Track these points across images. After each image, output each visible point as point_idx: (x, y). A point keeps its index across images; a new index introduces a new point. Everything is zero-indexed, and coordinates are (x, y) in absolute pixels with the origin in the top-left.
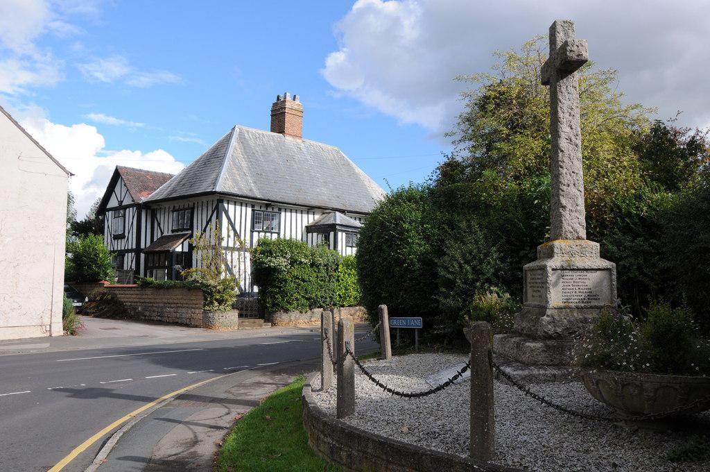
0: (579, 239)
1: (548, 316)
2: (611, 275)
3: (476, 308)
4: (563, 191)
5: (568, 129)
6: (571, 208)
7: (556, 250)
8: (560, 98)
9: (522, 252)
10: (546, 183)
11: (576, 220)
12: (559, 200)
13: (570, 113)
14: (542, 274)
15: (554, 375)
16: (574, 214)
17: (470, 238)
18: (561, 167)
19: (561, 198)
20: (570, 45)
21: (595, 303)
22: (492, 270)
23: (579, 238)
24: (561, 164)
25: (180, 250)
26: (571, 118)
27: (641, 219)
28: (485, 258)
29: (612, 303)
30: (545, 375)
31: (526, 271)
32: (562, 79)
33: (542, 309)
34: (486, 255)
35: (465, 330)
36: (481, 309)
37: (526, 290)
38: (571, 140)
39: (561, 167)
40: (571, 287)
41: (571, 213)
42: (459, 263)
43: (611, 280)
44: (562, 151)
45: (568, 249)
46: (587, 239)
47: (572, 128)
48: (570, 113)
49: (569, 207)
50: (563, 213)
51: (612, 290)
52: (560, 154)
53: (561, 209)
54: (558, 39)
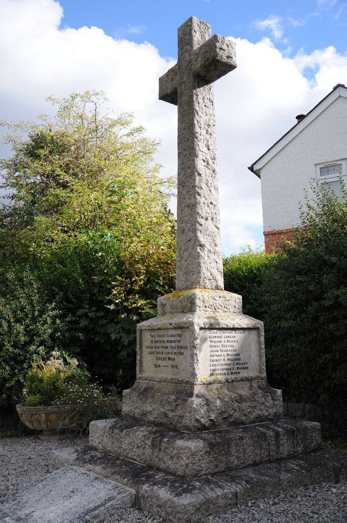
0: (218, 289)
1: (197, 396)
2: (259, 334)
3: (33, 379)
4: (201, 225)
5: (205, 149)
6: (210, 248)
7: (198, 302)
8: (197, 108)
9: (80, 311)
10: (109, 235)
11: (214, 265)
12: (196, 236)
13: (207, 131)
14: (180, 336)
15: (236, 494)
16: (212, 256)
17: (20, 292)
18: (199, 195)
19: (199, 234)
20: (220, 41)
21: (244, 374)
22: (49, 331)
23: (217, 288)
24: (199, 190)
25: (307, 405)
26: (208, 136)
27: (246, 277)
28: (40, 316)
29: (260, 372)
30: (225, 496)
31: (141, 331)
32: (199, 87)
33: (184, 389)
34: (42, 312)
35: (19, 408)
36: (41, 380)
37: (141, 357)
38: (208, 164)
39: (199, 195)
40: (219, 353)
41: (210, 255)
42: (9, 322)
43: (259, 343)
44: (200, 175)
45: (211, 301)
46: (226, 289)
47: (209, 149)
48: (207, 131)
49: (208, 246)
50: (202, 254)
51: (260, 356)
52: (197, 178)
53: (199, 248)
54: (195, 39)
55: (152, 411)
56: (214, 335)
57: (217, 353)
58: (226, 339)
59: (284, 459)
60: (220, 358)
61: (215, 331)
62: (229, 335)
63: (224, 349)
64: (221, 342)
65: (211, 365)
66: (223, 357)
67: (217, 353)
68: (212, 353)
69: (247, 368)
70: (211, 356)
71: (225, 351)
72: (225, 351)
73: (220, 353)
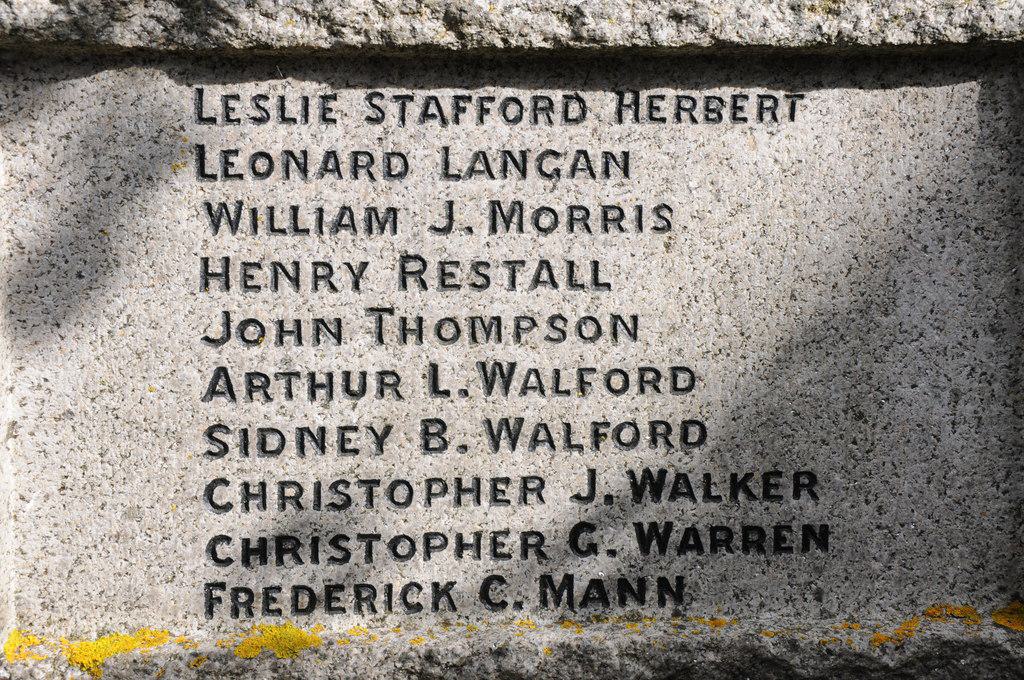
40: (361, 354)
55: (961, 26)
56: (274, 138)
57: (311, 358)
58: (480, 183)
59: (475, 162)
60: (371, 409)
61: (294, 90)
62: (530, 137)
63: (435, 304)
64: (383, 220)
65: (231, 494)
66: (418, 404)
67: (311, 358)
68: (239, 358)
69: (817, 536)
70: (220, 384)
71: (448, 330)
72: (448, 330)
73: (375, 360)
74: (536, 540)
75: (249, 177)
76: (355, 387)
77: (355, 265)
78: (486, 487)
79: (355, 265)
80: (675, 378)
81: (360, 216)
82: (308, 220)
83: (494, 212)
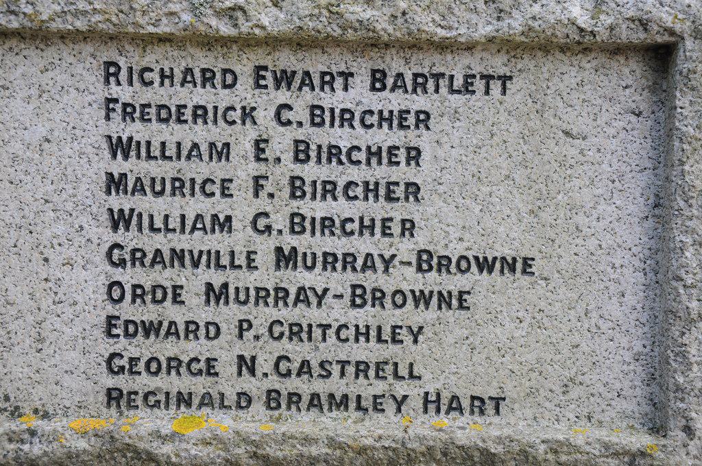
74: (283, 294)
75: (144, 374)
76: (309, 263)
77: (387, 257)
78: (378, 224)
79: (387, 257)
80: (154, 293)
81: (204, 148)
82: (174, 223)
83: (211, 150)
